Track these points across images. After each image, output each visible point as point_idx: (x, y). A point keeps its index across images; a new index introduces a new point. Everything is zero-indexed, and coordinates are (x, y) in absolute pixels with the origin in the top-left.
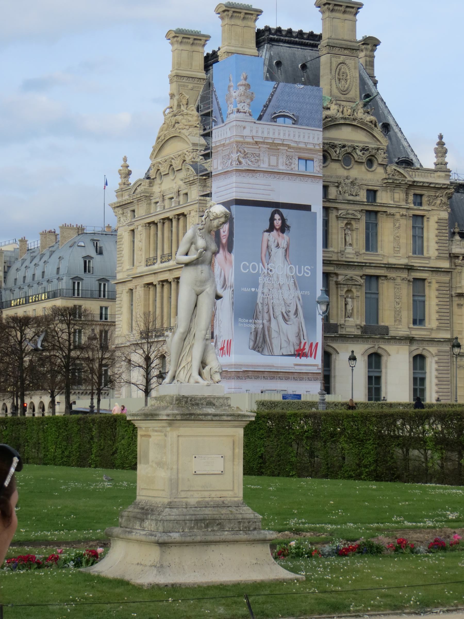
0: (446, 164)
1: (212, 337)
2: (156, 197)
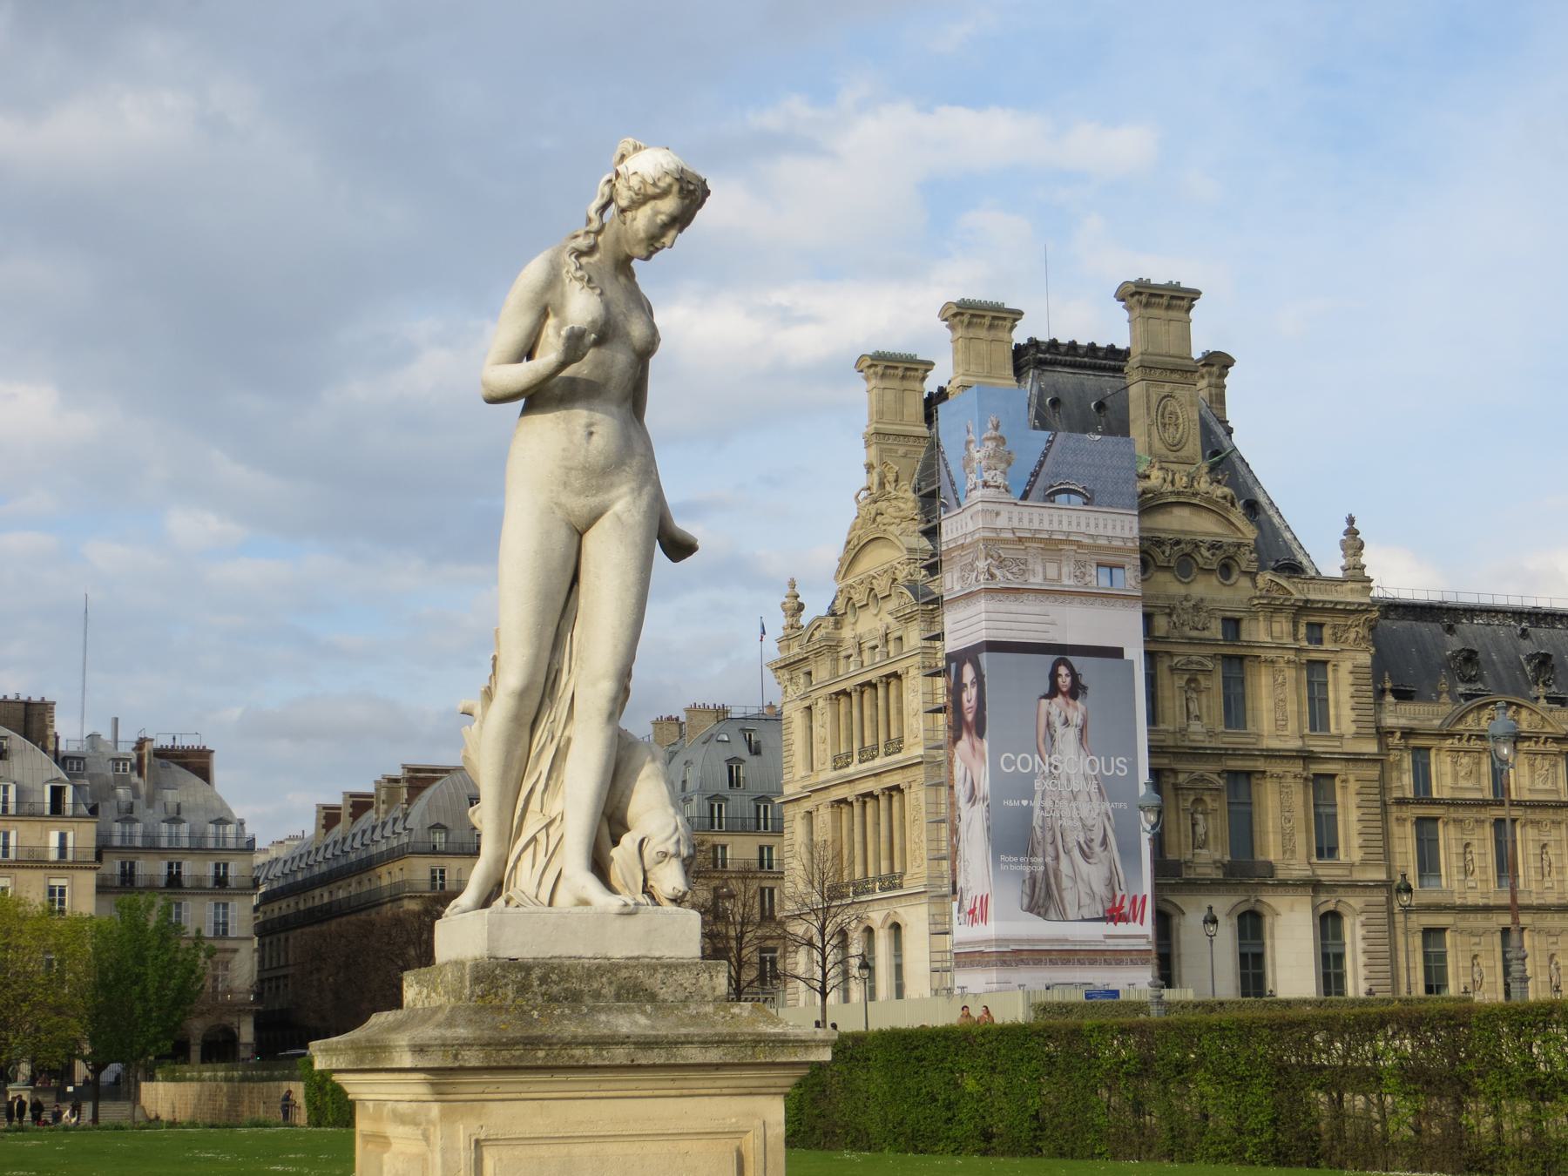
0: (1363, 567)
1: (954, 892)
2: (848, 646)
